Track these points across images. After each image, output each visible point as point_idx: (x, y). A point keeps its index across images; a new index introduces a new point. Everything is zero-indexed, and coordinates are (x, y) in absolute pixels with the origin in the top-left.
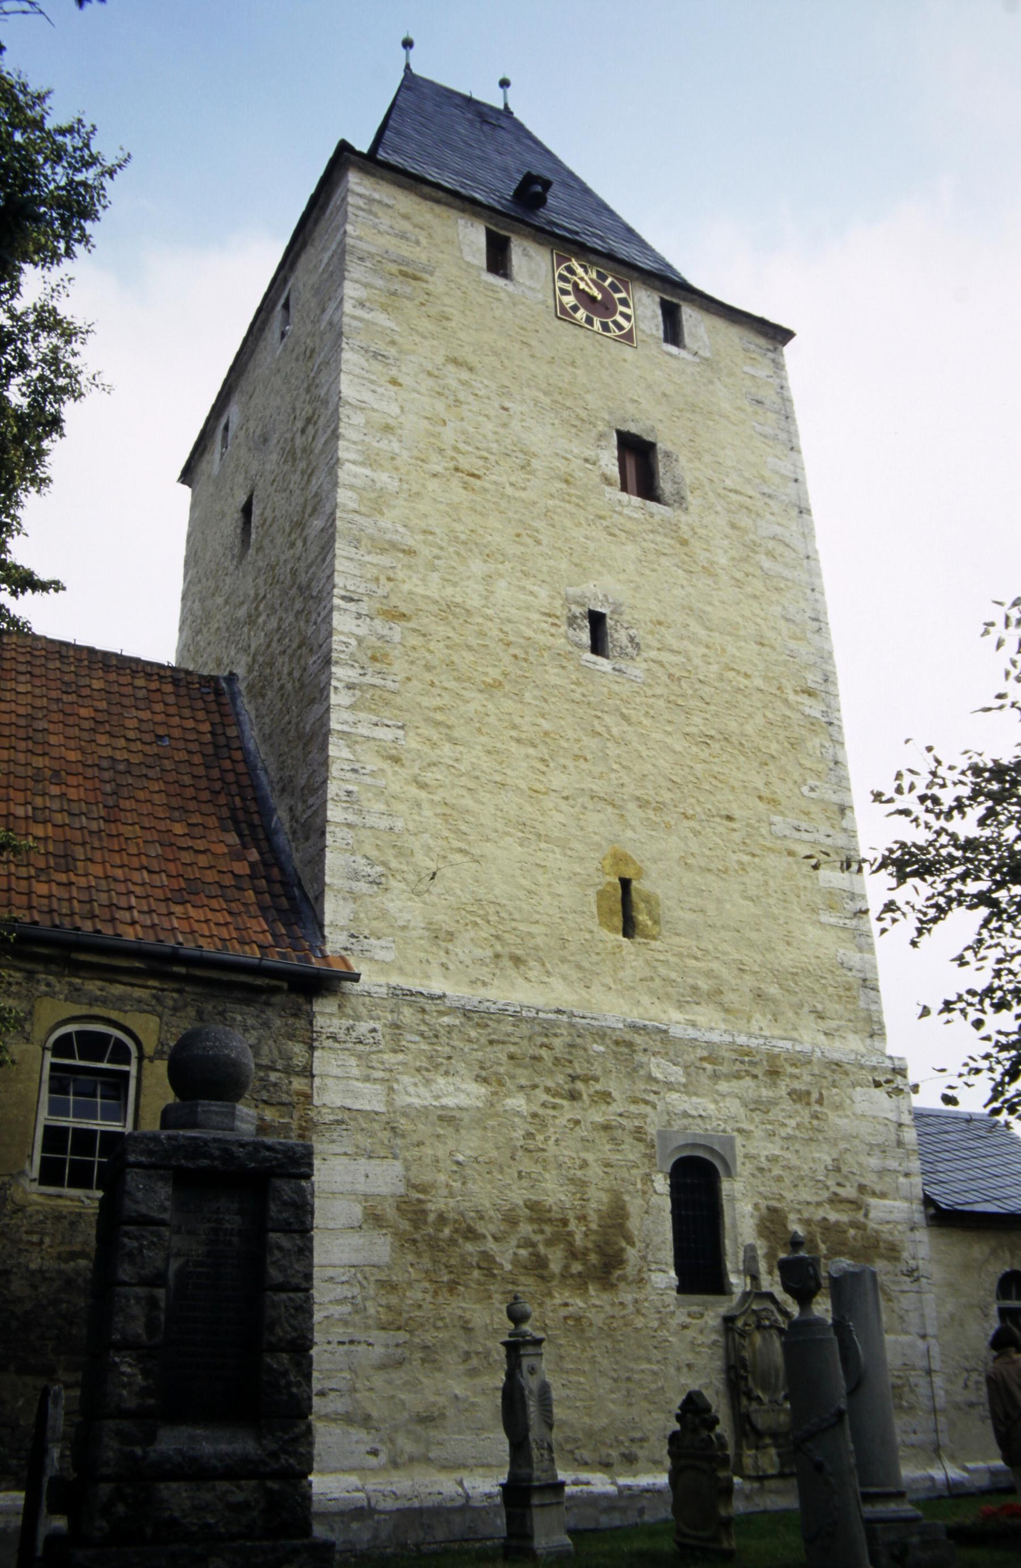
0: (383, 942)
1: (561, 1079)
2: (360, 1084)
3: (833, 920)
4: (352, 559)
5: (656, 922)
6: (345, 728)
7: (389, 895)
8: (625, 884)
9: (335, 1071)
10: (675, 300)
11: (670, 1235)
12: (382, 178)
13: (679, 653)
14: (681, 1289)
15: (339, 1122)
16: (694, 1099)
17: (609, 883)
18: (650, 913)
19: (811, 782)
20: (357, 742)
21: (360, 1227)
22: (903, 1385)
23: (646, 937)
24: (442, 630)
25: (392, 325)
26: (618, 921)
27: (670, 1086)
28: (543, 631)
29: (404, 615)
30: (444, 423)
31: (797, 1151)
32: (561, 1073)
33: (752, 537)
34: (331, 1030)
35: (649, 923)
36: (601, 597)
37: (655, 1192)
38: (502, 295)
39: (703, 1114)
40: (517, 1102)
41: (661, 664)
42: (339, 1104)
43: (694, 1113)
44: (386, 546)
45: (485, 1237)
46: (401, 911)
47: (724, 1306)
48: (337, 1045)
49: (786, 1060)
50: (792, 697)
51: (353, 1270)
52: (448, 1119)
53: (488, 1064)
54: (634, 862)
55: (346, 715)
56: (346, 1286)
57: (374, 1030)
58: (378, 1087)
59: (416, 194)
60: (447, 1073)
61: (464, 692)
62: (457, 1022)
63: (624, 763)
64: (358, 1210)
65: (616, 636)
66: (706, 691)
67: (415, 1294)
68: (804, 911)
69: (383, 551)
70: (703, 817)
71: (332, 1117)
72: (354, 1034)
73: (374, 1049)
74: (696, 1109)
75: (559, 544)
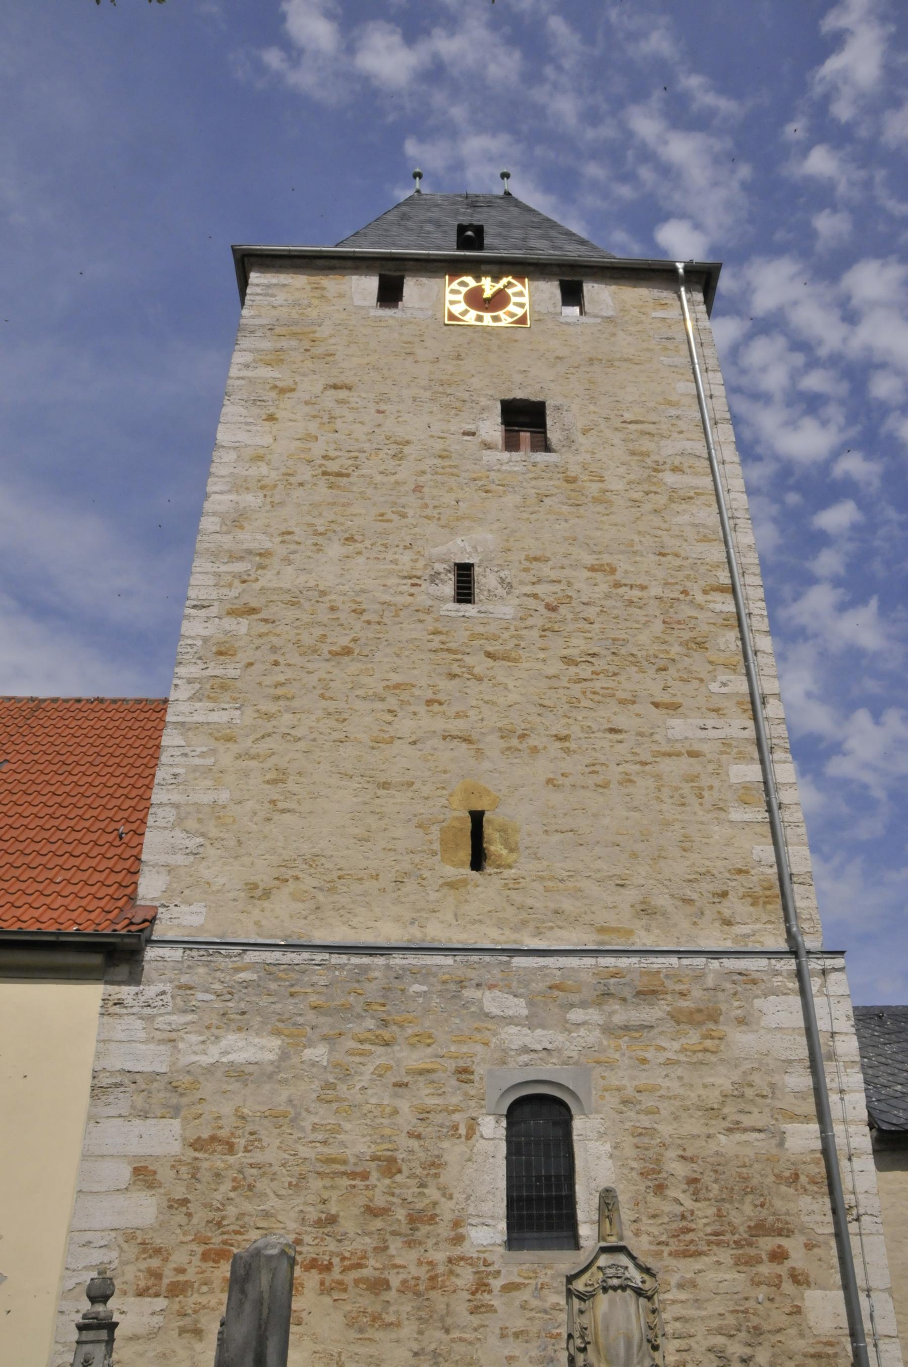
0: (193, 908)
1: (370, 1023)
2: (143, 1047)
3: (748, 817)
4: (207, 573)
5: (512, 850)
6: (180, 719)
7: (204, 863)
8: (477, 818)
9: (122, 1036)
10: (576, 279)
11: (502, 1184)
12: (281, 267)
13: (560, 582)
14: (512, 1243)
15: (117, 1085)
16: (539, 1032)
17: (457, 818)
18: (506, 843)
19: (724, 678)
20: (189, 729)
21: (127, 1189)
22: (836, 1355)
23: (499, 867)
24: (290, 614)
25: (276, 375)
26: (466, 854)
27: (511, 1020)
28: (401, 593)
29: (254, 609)
30: (316, 438)
31: (680, 1078)
32: (373, 1017)
33: (654, 457)
34: (119, 996)
35: (504, 852)
36: (469, 549)
37: (482, 1136)
38: (391, 322)
39: (549, 1047)
40: (318, 1053)
41: (535, 596)
42: (118, 1068)
43: (539, 1047)
44: (243, 554)
45: (266, 1195)
46: (216, 876)
47: (565, 1262)
48: (124, 1011)
49: (667, 976)
50: (700, 598)
51: (113, 1234)
52: (238, 1074)
53: (286, 1016)
54: (488, 792)
55: (184, 707)
56: (103, 1250)
57: (163, 993)
58: (162, 1047)
59: (314, 269)
60: (240, 1029)
61: (309, 665)
62: (255, 977)
63: (486, 698)
64: (125, 1173)
65: (483, 581)
66: (591, 612)
67: (179, 1258)
68: (709, 811)
69: (241, 558)
70: (582, 735)
71: (110, 1081)
72: (143, 999)
73: (162, 1010)
74: (540, 1042)
75: (429, 512)
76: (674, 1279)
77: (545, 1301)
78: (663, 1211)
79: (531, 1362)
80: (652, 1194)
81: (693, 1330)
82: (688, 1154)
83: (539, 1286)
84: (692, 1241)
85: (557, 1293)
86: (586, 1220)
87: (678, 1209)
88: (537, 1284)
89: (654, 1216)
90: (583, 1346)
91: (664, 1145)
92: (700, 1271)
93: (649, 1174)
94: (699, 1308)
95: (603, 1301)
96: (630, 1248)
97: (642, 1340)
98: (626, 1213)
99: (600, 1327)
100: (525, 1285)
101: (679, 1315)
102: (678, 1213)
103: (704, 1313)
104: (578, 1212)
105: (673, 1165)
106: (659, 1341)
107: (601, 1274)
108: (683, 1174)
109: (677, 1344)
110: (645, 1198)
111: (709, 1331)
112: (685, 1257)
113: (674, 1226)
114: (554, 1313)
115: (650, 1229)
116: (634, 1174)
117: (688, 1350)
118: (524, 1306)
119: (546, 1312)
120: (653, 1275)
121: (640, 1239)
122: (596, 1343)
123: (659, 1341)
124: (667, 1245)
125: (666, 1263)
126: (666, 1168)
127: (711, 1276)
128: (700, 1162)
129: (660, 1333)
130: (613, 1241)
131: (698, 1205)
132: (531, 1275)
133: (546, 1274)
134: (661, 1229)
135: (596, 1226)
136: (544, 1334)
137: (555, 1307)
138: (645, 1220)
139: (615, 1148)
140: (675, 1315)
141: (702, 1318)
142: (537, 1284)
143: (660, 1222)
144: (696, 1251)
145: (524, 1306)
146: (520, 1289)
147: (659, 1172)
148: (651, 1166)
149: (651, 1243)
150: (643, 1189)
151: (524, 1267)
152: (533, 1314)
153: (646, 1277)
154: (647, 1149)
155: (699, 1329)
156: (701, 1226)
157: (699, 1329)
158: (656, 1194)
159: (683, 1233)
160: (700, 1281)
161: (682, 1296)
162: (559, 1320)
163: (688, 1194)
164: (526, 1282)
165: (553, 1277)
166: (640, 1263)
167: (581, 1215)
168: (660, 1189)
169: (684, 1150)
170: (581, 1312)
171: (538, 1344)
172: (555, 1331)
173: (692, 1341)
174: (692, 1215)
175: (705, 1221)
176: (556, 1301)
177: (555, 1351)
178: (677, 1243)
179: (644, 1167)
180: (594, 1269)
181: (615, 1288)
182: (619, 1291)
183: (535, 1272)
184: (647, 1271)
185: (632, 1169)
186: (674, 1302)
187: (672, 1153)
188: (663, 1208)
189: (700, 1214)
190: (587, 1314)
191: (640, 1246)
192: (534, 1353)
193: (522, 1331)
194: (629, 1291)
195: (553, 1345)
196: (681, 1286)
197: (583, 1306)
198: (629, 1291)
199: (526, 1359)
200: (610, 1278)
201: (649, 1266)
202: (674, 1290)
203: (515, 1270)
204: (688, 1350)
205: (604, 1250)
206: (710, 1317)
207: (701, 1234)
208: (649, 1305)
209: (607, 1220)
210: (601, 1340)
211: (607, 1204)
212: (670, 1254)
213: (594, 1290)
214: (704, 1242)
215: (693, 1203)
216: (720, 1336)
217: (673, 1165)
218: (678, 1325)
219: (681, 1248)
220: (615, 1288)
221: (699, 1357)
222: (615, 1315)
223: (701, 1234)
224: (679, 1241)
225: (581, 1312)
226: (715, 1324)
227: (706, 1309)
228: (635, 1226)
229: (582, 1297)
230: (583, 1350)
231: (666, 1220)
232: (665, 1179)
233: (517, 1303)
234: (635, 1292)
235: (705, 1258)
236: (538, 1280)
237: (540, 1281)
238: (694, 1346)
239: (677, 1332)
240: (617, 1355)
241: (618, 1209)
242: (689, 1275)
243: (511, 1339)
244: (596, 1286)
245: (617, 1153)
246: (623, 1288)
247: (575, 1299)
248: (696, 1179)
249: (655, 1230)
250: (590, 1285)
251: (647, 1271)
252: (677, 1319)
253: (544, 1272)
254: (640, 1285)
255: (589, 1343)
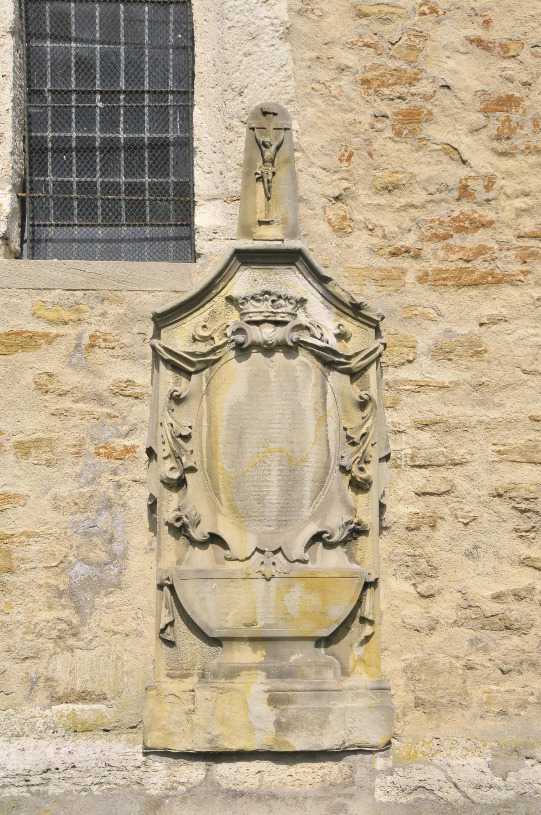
76: (426, 337)
77: (99, 375)
78: (413, 176)
79: (56, 508)
80: (389, 133)
81: (462, 451)
82: (496, 35)
83: (86, 341)
84: (481, 250)
85: (131, 358)
86: (215, 192)
87: (455, 174)
88: (79, 337)
89: (390, 188)
90: (175, 475)
91: (433, 11)
92: (495, 321)
93: (383, 84)
94: (483, 403)
95: (234, 376)
96: (311, 256)
97: (327, 467)
98: (313, 176)
99: (222, 435)
100: (50, 339)
101: (430, 417)
102: (453, 182)
103: (494, 414)
104: (198, 174)
105: (451, 64)
106: (370, 471)
107: (235, 315)
108: (476, 86)
109: (420, 478)
110: (369, 142)
111: (503, 454)
112: (459, 286)
113: (441, 212)
114: (123, 403)
115: (375, 218)
116: (346, 82)
117: (447, 492)
118: (45, 386)
119: (100, 400)
120: (375, 326)
121: (348, 240)
122: (211, 471)
123: (370, 471)
124: (416, 257)
125: (409, 299)
126: (432, 70)
127: (521, 332)
128: (525, 55)
129: (375, 454)
130: (270, 237)
131: (507, 164)
132: (66, 315)
133: (103, 315)
134: (405, 219)
135: (234, 208)
136: (92, 449)
137: (125, 390)
138: (364, 195)
139: (300, 13)
140: (419, 417)
141: (488, 426)
142: (79, 337)
143: (403, 201)
144: (491, 274)
145: (45, 386)
146: (37, 346)
147: (413, 81)
148: (393, 64)
149: (375, 251)
150: (366, 119)
151: (48, 297)
152: (66, 403)
153: (350, 326)
154: (386, 20)
155: (479, 450)
156: (508, 215)
157: (479, 450)
158: (399, 134)
159: (462, 229)
160: (489, 339)
161: (445, 374)
162: (132, 420)
163: (484, 135)
164: (54, 330)
165: (121, 322)
166: (337, 291)
167: (202, 183)
168: (411, 123)
169: (487, 23)
170: (177, 400)
171: (78, 469)
172: (119, 443)
173: (456, 475)
174: (488, 188)
175: (520, 203)
176: (126, 377)
177: (119, 486)
178: (441, 254)
179: (375, 67)
180: (219, 302)
181: (268, 349)
182: (279, 356)
183: (75, 307)
184: (355, 310)
185: (342, 69)
186: (417, 390)
187: (451, 33)
188: (415, 169)
189: (510, 185)
190: (191, 406)
191: (348, 260)
192: (65, 489)
193: (39, 440)
194: (303, 357)
195: (115, 473)
196: (443, 353)
197: (183, 386)
198: (303, 357)
199: (45, 502)
200: (257, 323)
201: (359, 299)
202: (424, 362)
203: (27, 303)
204: (447, 492)
205: (245, 257)
206: (510, 423)
207: (508, 235)
208: (355, 392)
209: (260, 187)
210: (223, 464)
211: (263, 146)
212: (422, 279)
213: (213, 351)
214: (511, 254)
215: (495, 159)
216: (528, 466)
217: (451, 64)
218: (426, 437)
219: (452, 266)
220: (268, 349)
221: (470, 508)
222: (274, 410)
223: (508, 235)
224: (449, 249)
225: (177, 400)
226: (518, 439)
227: (501, 405)
228: (335, 211)
229: (180, 365)
230: (180, 484)
231: (420, 197)
232: (426, 98)
233: (29, 377)
234: (319, 358)
235: (509, 290)
236: (82, 327)
237: (90, 330)
238: (463, 485)
239: (423, 453)
240: (261, 499)
241: (290, 161)
242: (463, 330)
243: (11, 458)
244: (218, 342)
245: (303, 26)
246: (290, 349)
247: (162, 366)
248: (510, 98)
249: (388, 222)
250: (205, 339)
251: (355, 310)
252: (424, 426)
253: (100, 308)
254: (334, 344)
255: (192, 470)
